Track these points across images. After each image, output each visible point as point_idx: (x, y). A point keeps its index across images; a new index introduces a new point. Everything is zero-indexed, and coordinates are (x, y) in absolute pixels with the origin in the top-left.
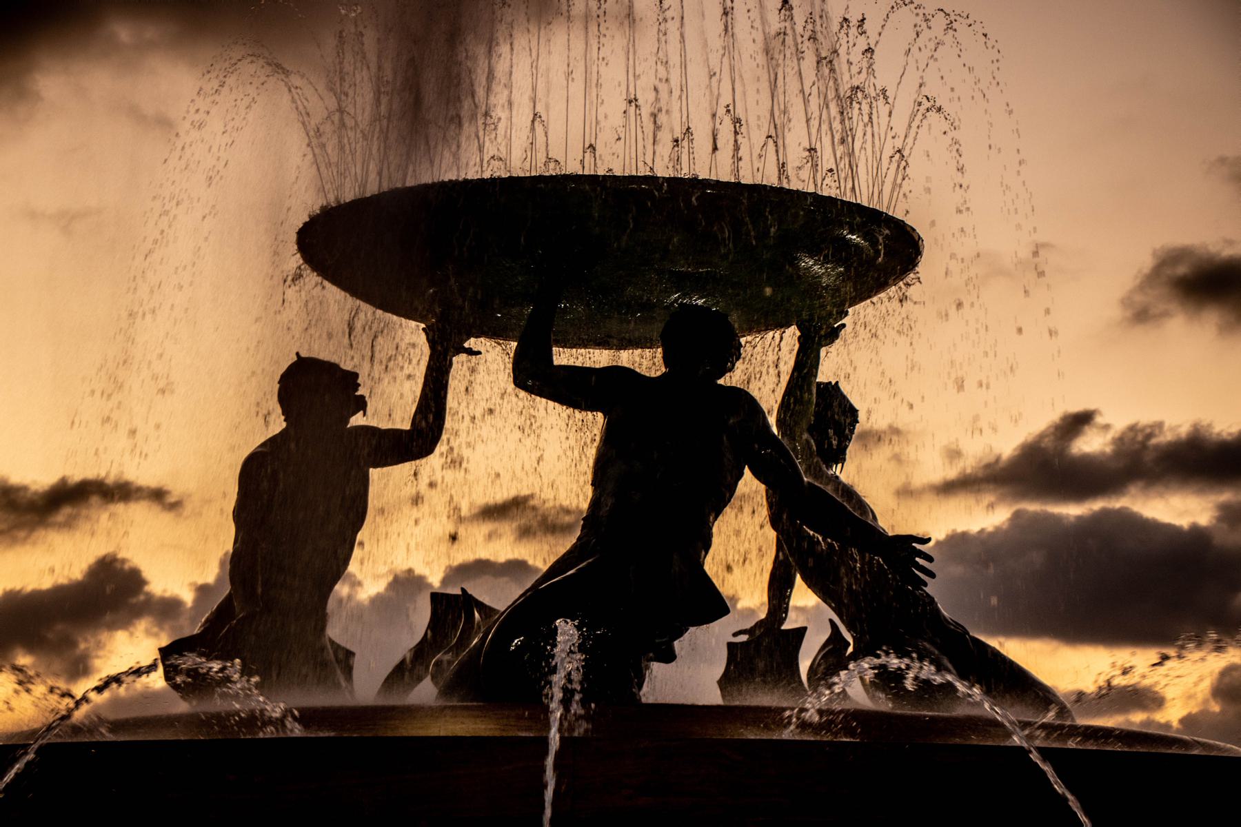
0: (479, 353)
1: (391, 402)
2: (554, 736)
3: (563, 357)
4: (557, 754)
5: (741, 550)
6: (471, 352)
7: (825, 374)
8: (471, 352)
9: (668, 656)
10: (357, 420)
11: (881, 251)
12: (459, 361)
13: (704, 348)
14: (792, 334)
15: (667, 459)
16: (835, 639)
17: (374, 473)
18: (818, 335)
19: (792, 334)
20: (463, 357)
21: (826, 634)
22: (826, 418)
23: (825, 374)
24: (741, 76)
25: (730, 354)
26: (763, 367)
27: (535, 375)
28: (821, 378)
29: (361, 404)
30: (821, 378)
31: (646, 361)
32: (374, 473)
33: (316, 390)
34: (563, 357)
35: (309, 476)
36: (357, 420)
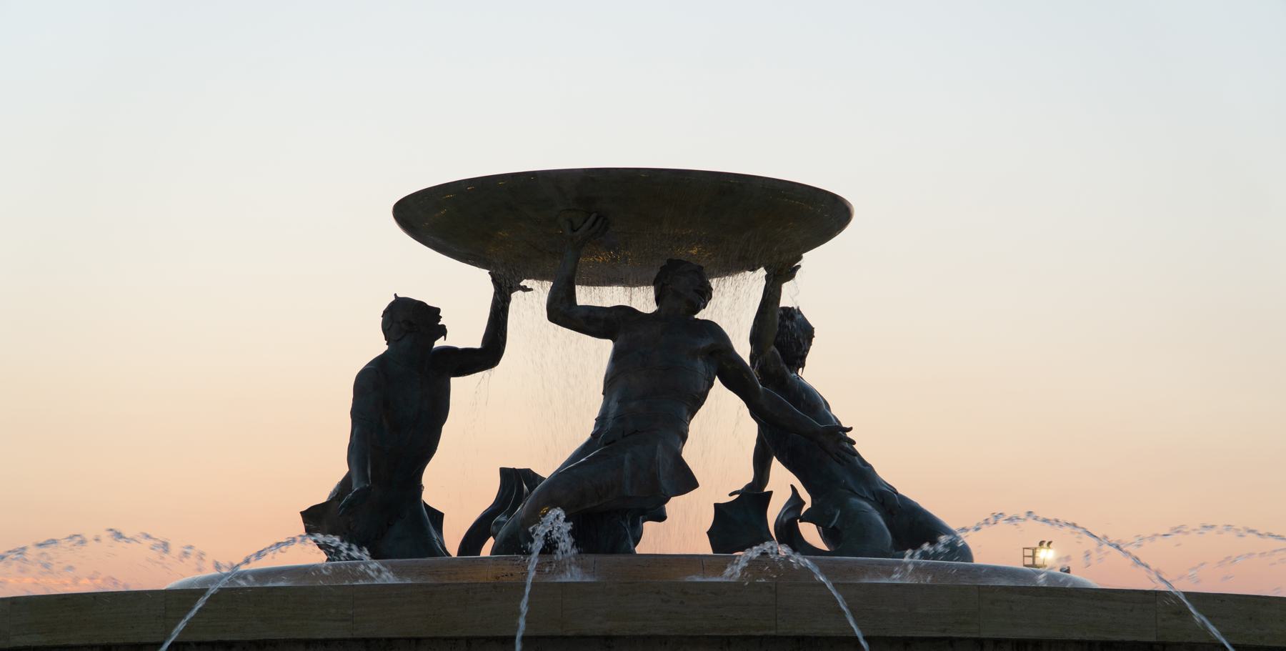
0: (531, 290)
1: (464, 330)
2: (529, 581)
3: (586, 296)
4: (522, 597)
5: (721, 438)
6: (525, 289)
7: (785, 302)
8: (525, 289)
9: (661, 517)
10: (439, 343)
11: (820, 214)
12: (517, 297)
13: (682, 291)
14: (762, 272)
15: (657, 375)
16: (796, 500)
17: (453, 380)
18: (782, 272)
19: (762, 272)
20: (519, 293)
21: (789, 493)
22: (784, 335)
23: (785, 302)
24: (259, 555)
25: (704, 295)
26: (733, 305)
27: (562, 311)
28: (782, 305)
29: (442, 331)
30: (782, 305)
31: (643, 300)
32: (453, 380)
33: (411, 322)
34: (586, 296)
35: (409, 382)
36: (439, 343)
